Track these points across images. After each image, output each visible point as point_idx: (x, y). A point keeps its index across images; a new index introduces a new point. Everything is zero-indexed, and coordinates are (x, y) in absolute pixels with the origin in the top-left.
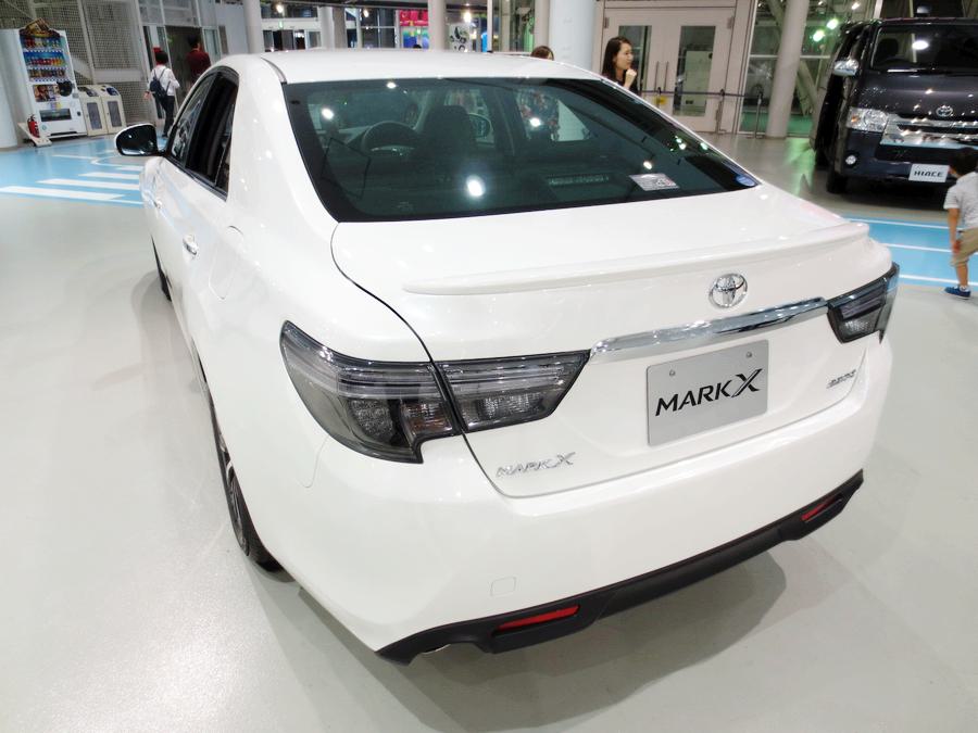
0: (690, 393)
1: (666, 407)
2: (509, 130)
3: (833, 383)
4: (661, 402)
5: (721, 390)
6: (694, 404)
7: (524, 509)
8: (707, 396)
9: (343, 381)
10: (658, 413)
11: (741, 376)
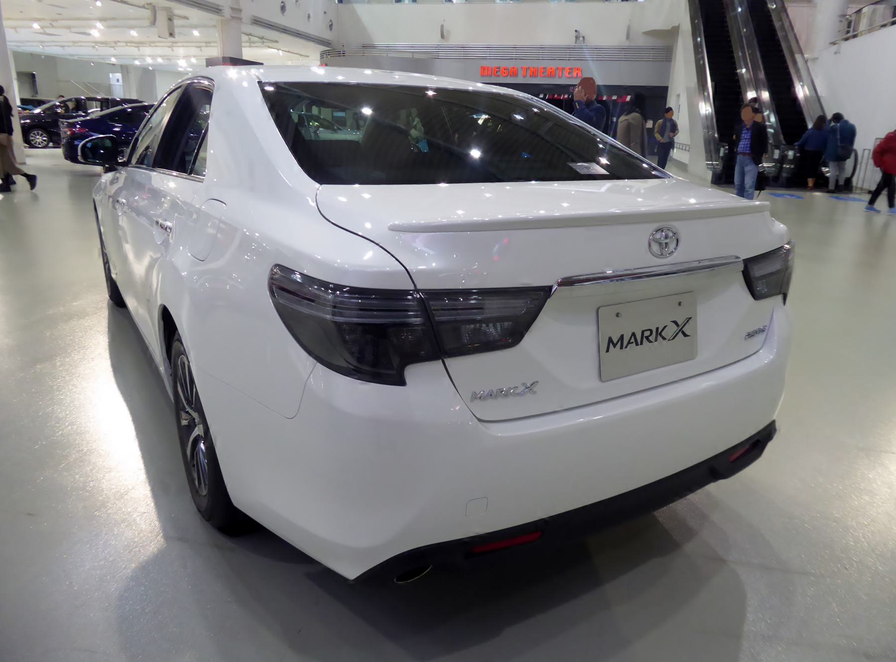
0: (634, 334)
1: (615, 345)
2: (480, 86)
3: (750, 335)
4: (610, 340)
5: (659, 333)
6: (637, 344)
7: (500, 431)
8: (647, 338)
9: (481, 308)
10: (607, 351)
11: (675, 323)
